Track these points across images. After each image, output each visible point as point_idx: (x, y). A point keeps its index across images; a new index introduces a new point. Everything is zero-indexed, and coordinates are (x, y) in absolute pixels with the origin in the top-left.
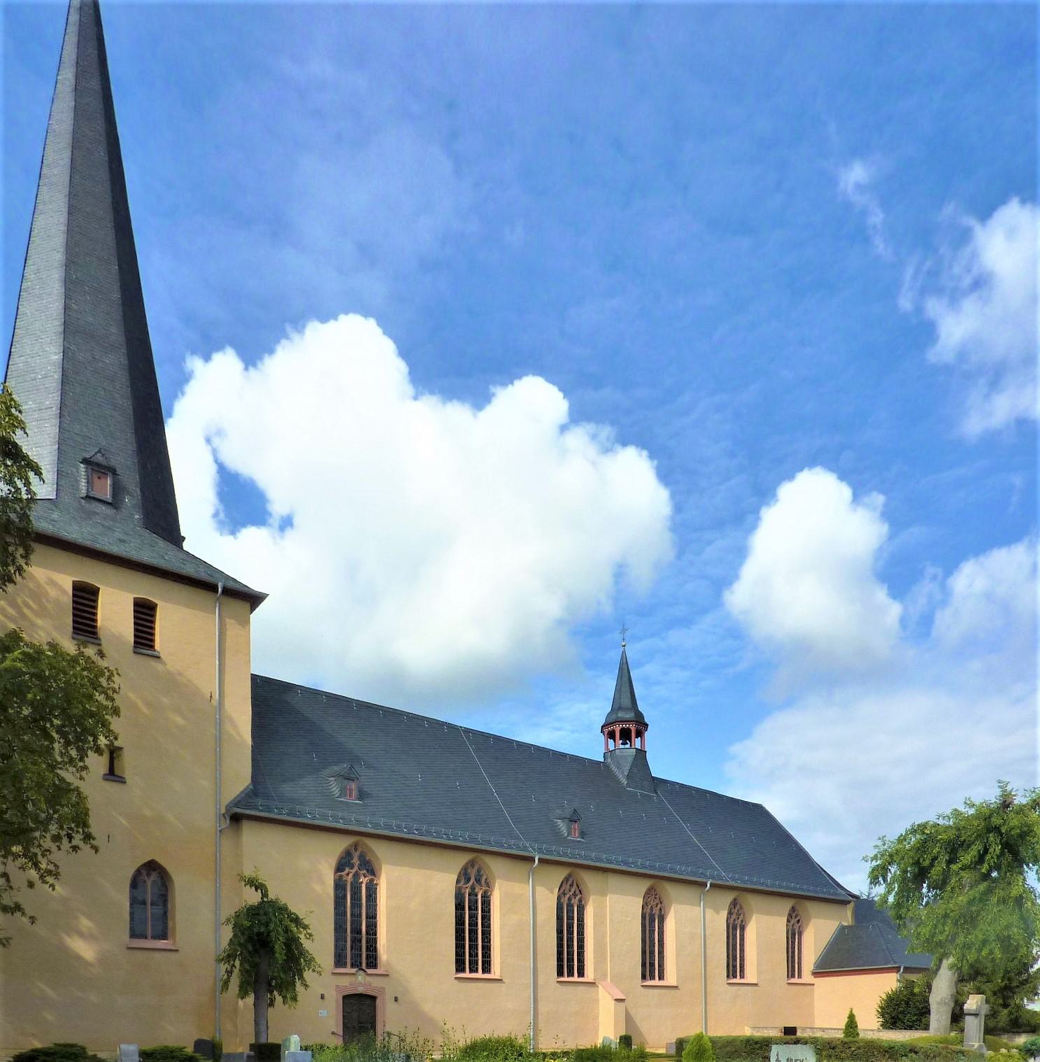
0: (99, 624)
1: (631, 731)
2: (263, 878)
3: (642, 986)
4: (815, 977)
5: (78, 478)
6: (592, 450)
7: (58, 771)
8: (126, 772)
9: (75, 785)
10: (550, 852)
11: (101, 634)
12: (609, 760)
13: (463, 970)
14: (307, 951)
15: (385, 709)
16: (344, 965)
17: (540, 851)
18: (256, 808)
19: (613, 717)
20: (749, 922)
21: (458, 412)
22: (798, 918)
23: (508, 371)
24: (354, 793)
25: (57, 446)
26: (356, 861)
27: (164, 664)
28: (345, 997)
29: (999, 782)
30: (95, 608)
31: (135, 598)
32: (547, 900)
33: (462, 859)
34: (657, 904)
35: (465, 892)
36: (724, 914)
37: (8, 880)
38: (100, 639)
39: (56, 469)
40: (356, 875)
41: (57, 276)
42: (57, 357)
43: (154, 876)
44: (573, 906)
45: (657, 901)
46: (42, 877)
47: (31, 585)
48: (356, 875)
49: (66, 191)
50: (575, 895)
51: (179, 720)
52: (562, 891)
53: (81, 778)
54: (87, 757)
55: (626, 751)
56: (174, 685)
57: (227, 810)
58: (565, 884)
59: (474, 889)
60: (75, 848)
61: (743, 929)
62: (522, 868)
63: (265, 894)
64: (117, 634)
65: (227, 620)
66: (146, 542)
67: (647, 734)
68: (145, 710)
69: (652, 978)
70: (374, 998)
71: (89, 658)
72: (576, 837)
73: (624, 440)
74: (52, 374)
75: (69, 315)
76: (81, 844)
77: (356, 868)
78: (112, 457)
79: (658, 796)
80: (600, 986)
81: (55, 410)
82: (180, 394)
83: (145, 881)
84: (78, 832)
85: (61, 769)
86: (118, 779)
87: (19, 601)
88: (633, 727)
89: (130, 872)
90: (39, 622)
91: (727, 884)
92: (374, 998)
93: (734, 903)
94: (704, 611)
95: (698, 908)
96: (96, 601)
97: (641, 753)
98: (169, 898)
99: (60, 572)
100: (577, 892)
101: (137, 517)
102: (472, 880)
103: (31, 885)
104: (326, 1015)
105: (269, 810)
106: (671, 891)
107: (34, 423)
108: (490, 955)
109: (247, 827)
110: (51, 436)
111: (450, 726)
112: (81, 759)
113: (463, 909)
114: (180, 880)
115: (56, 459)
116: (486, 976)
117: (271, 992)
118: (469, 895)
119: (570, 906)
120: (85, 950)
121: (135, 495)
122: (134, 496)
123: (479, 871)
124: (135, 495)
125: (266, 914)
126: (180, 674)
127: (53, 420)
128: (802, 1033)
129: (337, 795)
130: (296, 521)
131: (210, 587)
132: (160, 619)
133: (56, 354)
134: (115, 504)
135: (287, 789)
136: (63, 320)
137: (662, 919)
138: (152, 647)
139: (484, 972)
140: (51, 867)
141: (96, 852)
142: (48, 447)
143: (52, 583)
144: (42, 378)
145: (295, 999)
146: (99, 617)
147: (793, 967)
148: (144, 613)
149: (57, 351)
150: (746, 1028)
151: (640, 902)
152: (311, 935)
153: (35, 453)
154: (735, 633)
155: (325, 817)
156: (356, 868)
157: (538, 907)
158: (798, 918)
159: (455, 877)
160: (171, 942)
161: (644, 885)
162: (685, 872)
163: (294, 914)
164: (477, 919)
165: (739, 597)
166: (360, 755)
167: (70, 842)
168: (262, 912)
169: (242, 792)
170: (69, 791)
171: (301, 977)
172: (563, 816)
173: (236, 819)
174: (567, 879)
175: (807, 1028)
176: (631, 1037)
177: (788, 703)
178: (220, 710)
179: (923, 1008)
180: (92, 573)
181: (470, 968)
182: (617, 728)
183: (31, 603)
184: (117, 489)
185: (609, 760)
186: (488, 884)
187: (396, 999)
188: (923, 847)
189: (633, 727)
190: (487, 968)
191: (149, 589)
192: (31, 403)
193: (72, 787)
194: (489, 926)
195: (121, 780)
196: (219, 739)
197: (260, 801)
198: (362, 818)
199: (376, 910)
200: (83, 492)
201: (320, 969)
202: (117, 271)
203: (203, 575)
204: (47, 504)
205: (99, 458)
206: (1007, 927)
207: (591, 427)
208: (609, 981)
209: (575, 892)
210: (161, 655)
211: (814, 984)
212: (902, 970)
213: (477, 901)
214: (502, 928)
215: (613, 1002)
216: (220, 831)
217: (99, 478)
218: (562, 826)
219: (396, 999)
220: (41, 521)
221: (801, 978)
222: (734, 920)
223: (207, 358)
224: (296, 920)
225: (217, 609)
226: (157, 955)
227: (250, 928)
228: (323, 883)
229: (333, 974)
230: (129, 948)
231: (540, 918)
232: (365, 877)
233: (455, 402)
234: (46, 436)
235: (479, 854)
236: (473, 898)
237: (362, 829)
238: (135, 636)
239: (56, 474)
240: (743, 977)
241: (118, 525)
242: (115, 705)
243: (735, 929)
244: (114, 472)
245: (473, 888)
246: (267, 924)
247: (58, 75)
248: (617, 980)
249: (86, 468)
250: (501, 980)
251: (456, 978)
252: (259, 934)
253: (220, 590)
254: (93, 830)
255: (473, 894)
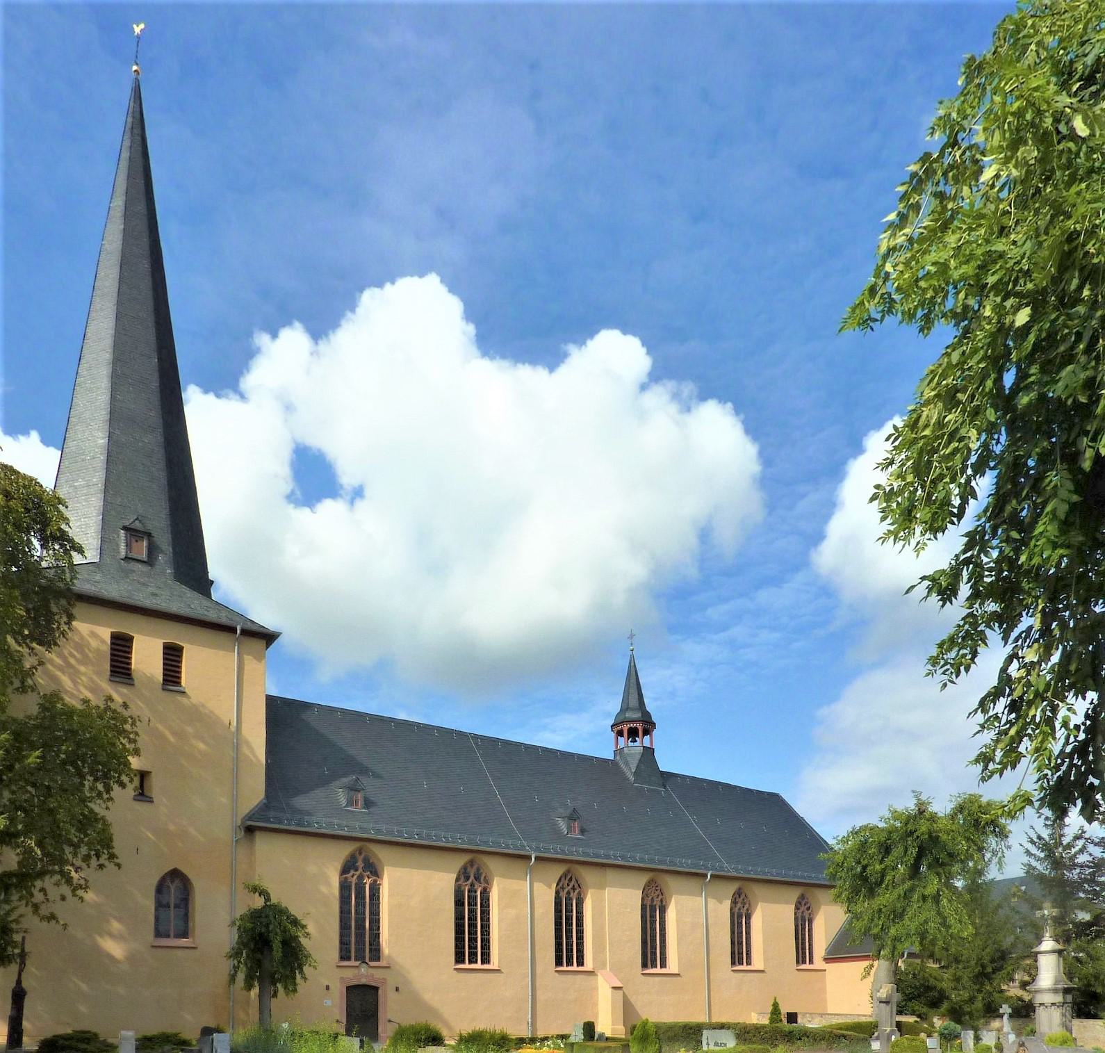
0: (133, 667)
1: (638, 730)
2: (267, 884)
3: (643, 974)
4: (827, 963)
5: (119, 543)
6: (673, 408)
7: (89, 804)
8: (154, 792)
9: (102, 815)
10: (547, 850)
11: (134, 675)
12: (618, 758)
13: (463, 962)
14: (305, 948)
15: (396, 721)
16: (348, 959)
17: (537, 849)
18: (268, 821)
19: (622, 718)
20: (755, 910)
21: (531, 376)
22: (808, 905)
23: (584, 330)
24: (360, 803)
25: (101, 517)
26: (360, 864)
27: (189, 698)
28: (348, 988)
29: (913, 792)
30: (130, 653)
31: (164, 643)
32: (545, 895)
33: (460, 861)
34: (658, 895)
35: (465, 889)
36: (727, 904)
37: (46, 894)
38: (132, 679)
39: (100, 536)
40: (361, 878)
41: (105, 372)
42: (103, 441)
43: (177, 882)
44: (571, 899)
45: (658, 892)
46: (74, 890)
47: (76, 639)
48: (361, 878)
49: (114, 300)
50: (574, 889)
51: (202, 746)
52: (561, 885)
53: (107, 808)
54: (112, 790)
55: (635, 748)
56: (198, 716)
57: (242, 823)
58: (563, 879)
59: (474, 886)
60: (101, 866)
61: (748, 917)
62: (519, 864)
63: (268, 899)
64: (149, 675)
65: (245, 656)
66: (175, 593)
67: (655, 733)
68: (172, 739)
69: (653, 965)
70: (376, 989)
71: (115, 710)
72: (576, 835)
73: (704, 396)
74: (99, 456)
75: (114, 405)
76: (106, 863)
77: (360, 870)
78: (148, 522)
79: (667, 790)
80: (599, 974)
81: (101, 486)
82: (245, 371)
83: (169, 887)
84: (103, 853)
85: (89, 802)
86: (148, 799)
87: (66, 652)
88: (640, 727)
89: (154, 881)
90: (82, 669)
91: (729, 874)
92: (376, 989)
93: (738, 893)
94: (797, 569)
95: (700, 898)
96: (131, 647)
97: (649, 752)
98: (190, 901)
99: (99, 625)
100: (576, 886)
101: (169, 571)
102: (472, 877)
103: (63, 898)
104: (330, 1004)
105: (280, 822)
106: (671, 883)
107: (83, 498)
108: (489, 946)
109: (259, 838)
110: (97, 508)
111: (460, 733)
112: (108, 792)
113: (463, 904)
114: (198, 885)
115: (100, 527)
116: (486, 966)
117: (275, 985)
118: (469, 892)
119: (569, 899)
120: (115, 949)
121: (168, 553)
122: (166, 554)
123: (478, 870)
124: (168, 553)
125: (267, 916)
126: (203, 706)
127: (99, 495)
128: (803, 1018)
129: (344, 805)
130: (367, 493)
131: (232, 630)
132: (186, 659)
133: (103, 438)
134: (150, 562)
135: (301, 802)
136: (109, 409)
137: (663, 910)
138: (179, 684)
139: (483, 963)
140: (82, 882)
141: (119, 868)
142: (94, 518)
143: (93, 634)
144: (91, 459)
145: (295, 991)
146: (133, 661)
147: (803, 953)
148: (172, 655)
149: (104, 436)
150: (753, 1014)
151: (639, 894)
152: (308, 934)
153: (83, 523)
154: (826, 591)
155: (330, 825)
156: (360, 870)
157: (536, 902)
158: (808, 905)
159: (454, 876)
160: (191, 940)
161: (643, 879)
162: (686, 864)
163: (293, 915)
164: (476, 914)
165: (827, 556)
166: (369, 766)
167: (98, 860)
168: (263, 915)
169: (256, 806)
170: (97, 820)
171: (301, 972)
172: (563, 815)
173: (250, 830)
174: (565, 875)
175: (806, 1013)
176: (593, 1023)
177: (878, 664)
178: (237, 734)
179: (910, 994)
180: (126, 624)
181: (469, 960)
182: (625, 728)
183: (76, 653)
184: (152, 549)
185: (618, 758)
186: (487, 881)
187: (397, 989)
188: (863, 846)
189: (640, 727)
190: (486, 959)
191: (176, 634)
192: (80, 480)
193: (99, 817)
194: (488, 920)
195: (150, 801)
196: (237, 759)
197: (272, 814)
198: (365, 825)
199: (379, 907)
200: (123, 554)
201: (316, 964)
202: (157, 364)
203: (224, 620)
204: (91, 567)
205: (137, 525)
206: (926, 922)
207: (671, 385)
208: (608, 969)
209: (574, 886)
210: (187, 691)
211: (825, 970)
212: (906, 956)
213: (476, 897)
214: (500, 921)
215: (611, 989)
216: (236, 841)
217: (137, 541)
218: (563, 825)
219: (397, 989)
220: (82, 585)
221: (812, 963)
222: (739, 909)
223: (274, 335)
224: (295, 922)
225: (236, 647)
226: (179, 953)
227: (253, 929)
228: (328, 884)
229: (338, 966)
230: (153, 947)
231: (538, 912)
232: (368, 878)
233: (527, 365)
234: (93, 509)
235: (365, 843)
236: (473, 894)
237: (365, 836)
238: (164, 675)
239: (100, 540)
240: (750, 964)
241: (151, 580)
242: (137, 746)
243: (740, 916)
244: (149, 535)
245: (472, 885)
246: (267, 926)
247: (111, 202)
248: (616, 970)
249: (126, 534)
250: (499, 970)
251: (456, 969)
252: (261, 935)
253: (238, 632)
254: (115, 851)
255: (472, 890)
